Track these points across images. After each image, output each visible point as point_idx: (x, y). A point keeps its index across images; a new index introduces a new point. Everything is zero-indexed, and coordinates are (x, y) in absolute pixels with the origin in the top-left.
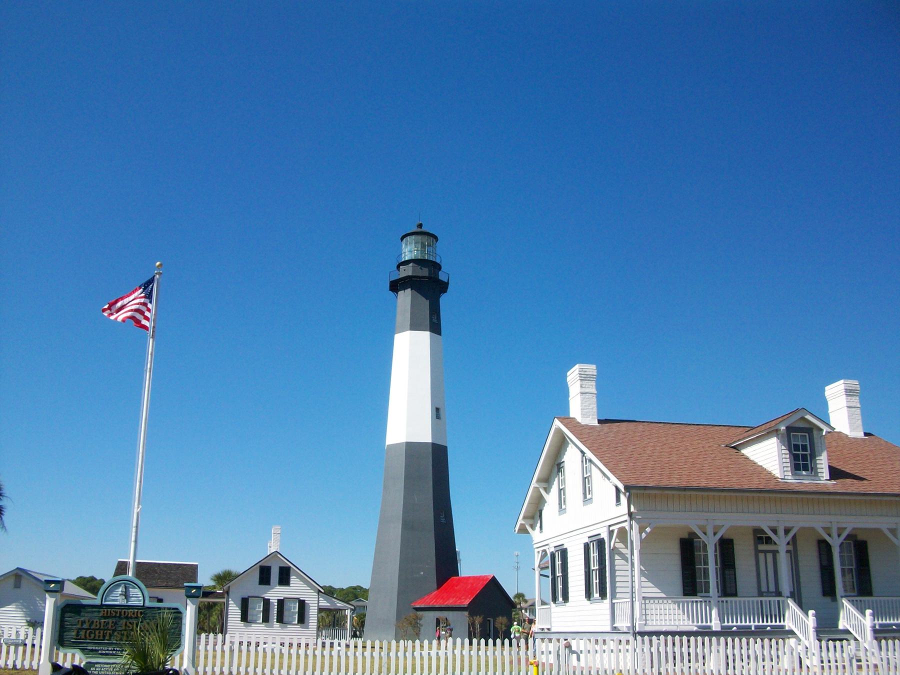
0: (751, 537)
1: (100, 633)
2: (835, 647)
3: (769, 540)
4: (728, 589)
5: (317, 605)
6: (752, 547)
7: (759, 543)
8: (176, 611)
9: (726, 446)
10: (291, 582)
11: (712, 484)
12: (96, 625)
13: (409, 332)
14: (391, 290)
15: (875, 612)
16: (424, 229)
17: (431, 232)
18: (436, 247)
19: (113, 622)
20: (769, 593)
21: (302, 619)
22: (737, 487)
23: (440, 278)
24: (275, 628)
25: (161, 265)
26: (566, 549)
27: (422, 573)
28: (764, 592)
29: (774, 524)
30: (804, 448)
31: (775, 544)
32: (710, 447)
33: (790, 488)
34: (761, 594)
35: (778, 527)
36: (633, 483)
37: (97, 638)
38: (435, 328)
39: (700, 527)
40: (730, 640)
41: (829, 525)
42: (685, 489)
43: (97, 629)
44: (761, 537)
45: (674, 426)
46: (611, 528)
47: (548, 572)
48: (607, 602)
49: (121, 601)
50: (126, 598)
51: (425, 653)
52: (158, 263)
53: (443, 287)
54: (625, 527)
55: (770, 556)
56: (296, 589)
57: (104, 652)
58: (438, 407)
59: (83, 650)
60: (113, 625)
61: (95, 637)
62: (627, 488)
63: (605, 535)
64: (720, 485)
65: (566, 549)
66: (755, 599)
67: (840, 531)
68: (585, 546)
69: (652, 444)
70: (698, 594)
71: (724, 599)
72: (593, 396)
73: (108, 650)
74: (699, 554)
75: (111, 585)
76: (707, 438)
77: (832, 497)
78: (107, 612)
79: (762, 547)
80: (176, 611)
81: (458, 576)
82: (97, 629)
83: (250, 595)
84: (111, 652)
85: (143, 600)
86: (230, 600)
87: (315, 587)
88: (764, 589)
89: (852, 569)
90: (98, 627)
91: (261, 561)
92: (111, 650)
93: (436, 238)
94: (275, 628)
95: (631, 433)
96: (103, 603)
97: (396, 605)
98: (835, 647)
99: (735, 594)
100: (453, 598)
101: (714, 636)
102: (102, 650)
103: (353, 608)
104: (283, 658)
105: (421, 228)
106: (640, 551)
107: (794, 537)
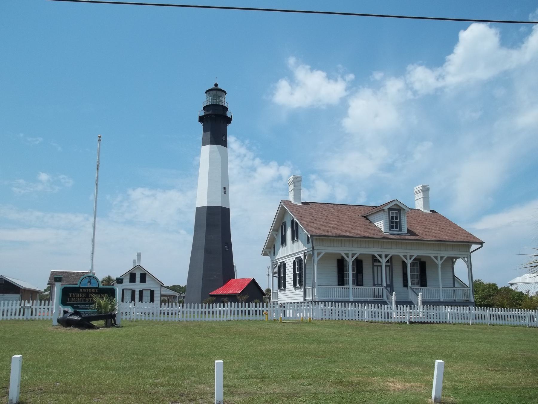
0: (371, 259)
1: (79, 299)
4: (359, 282)
6: (371, 264)
7: (375, 262)
9: (362, 216)
11: (351, 235)
12: (78, 296)
14: (199, 121)
20: (378, 285)
21: (152, 300)
22: (363, 236)
24: (288, 292)
27: (215, 277)
28: (376, 284)
30: (396, 218)
32: (354, 217)
33: (388, 237)
34: (374, 285)
35: (382, 254)
36: (314, 233)
39: (345, 254)
41: (405, 254)
42: (339, 237)
44: (375, 259)
45: (338, 205)
47: (277, 275)
50: (90, 284)
56: (149, 285)
57: (81, 307)
61: (77, 301)
62: (311, 235)
64: (355, 235)
66: (372, 287)
67: (411, 257)
68: (293, 262)
69: (326, 215)
70: (345, 285)
71: (358, 287)
76: (353, 212)
77: (407, 241)
79: (375, 264)
81: (235, 278)
83: (125, 288)
84: (84, 307)
87: (159, 283)
88: (376, 283)
89: (418, 274)
92: (85, 306)
93: (225, 93)
95: (317, 209)
97: (201, 294)
99: (362, 285)
100: (232, 290)
103: (163, 303)
106: (317, 264)
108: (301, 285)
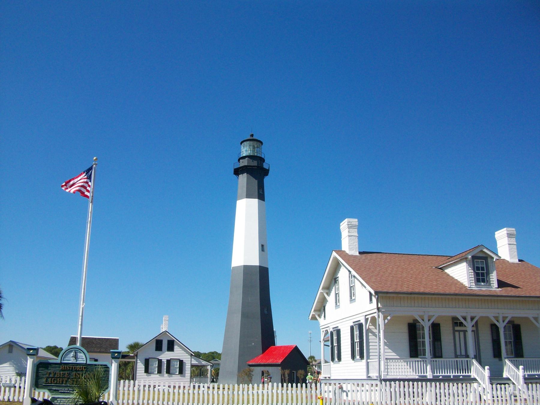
0: (451, 322)
1: (60, 380)
2: (501, 388)
3: (461, 324)
4: (437, 353)
5: (190, 363)
6: (451, 328)
7: (455, 326)
8: (105, 366)
9: (436, 268)
10: (175, 349)
11: (427, 290)
12: (58, 375)
13: (245, 199)
14: (234, 174)
15: (525, 367)
16: (254, 137)
17: (258, 139)
18: (262, 148)
19: (68, 373)
20: (461, 356)
21: (181, 371)
22: (442, 292)
23: (264, 167)
24: (165, 377)
25: (96, 159)
26: (340, 329)
27: (253, 344)
28: (458, 355)
29: (464, 314)
30: (483, 269)
31: (465, 326)
32: (426, 268)
33: (474, 293)
34: (456, 356)
35: (467, 316)
36: (380, 290)
37: (58, 383)
38: (261, 197)
39: (420, 316)
40: (438, 384)
41: (497, 315)
42: (411, 293)
43: (58, 378)
44: (456, 322)
45: (404, 255)
46: (367, 317)
47: (329, 343)
48: (364, 361)
49: (72, 360)
50: (75, 359)
51: (255, 392)
52: (95, 158)
53: (266, 172)
54: (375, 316)
55: (462, 334)
56: (178, 353)
57: (62, 391)
58: (263, 244)
59: (50, 390)
60: (68, 375)
61: (57, 382)
63: (363, 321)
64: (432, 291)
65: (340, 329)
66: (453, 359)
67: (504, 318)
68: (351, 328)
69: (391, 266)
70: (419, 356)
71: (435, 359)
72: (356, 238)
73: (65, 390)
74: (419, 332)
75: (66, 351)
76: (424, 263)
77: (499, 298)
78: (64, 367)
79: (457, 328)
80: (105, 366)
81: (275, 345)
82: (58, 378)
83: (150, 357)
84: (67, 391)
85: (86, 360)
86: (138, 360)
87: (189, 352)
88: (458, 353)
89: (511, 341)
90: (59, 376)
91: (157, 336)
92: (67, 390)
93: (261, 143)
94: (165, 377)
95: (379, 260)
96: (62, 362)
97: (238, 363)
98: (501, 388)
99: (441, 357)
100: (272, 359)
101: (429, 382)
102: (61, 390)
104: (170, 395)
105: (253, 137)
106: (384, 330)
107: (476, 322)
108: (362, 357)
